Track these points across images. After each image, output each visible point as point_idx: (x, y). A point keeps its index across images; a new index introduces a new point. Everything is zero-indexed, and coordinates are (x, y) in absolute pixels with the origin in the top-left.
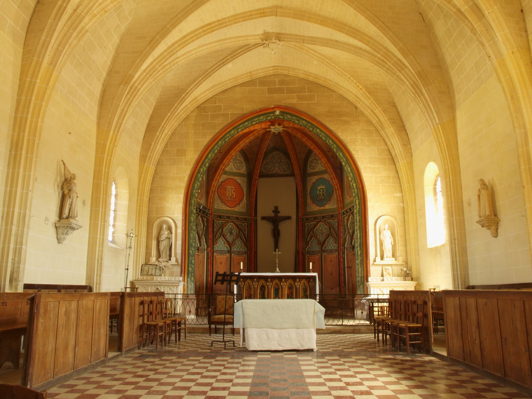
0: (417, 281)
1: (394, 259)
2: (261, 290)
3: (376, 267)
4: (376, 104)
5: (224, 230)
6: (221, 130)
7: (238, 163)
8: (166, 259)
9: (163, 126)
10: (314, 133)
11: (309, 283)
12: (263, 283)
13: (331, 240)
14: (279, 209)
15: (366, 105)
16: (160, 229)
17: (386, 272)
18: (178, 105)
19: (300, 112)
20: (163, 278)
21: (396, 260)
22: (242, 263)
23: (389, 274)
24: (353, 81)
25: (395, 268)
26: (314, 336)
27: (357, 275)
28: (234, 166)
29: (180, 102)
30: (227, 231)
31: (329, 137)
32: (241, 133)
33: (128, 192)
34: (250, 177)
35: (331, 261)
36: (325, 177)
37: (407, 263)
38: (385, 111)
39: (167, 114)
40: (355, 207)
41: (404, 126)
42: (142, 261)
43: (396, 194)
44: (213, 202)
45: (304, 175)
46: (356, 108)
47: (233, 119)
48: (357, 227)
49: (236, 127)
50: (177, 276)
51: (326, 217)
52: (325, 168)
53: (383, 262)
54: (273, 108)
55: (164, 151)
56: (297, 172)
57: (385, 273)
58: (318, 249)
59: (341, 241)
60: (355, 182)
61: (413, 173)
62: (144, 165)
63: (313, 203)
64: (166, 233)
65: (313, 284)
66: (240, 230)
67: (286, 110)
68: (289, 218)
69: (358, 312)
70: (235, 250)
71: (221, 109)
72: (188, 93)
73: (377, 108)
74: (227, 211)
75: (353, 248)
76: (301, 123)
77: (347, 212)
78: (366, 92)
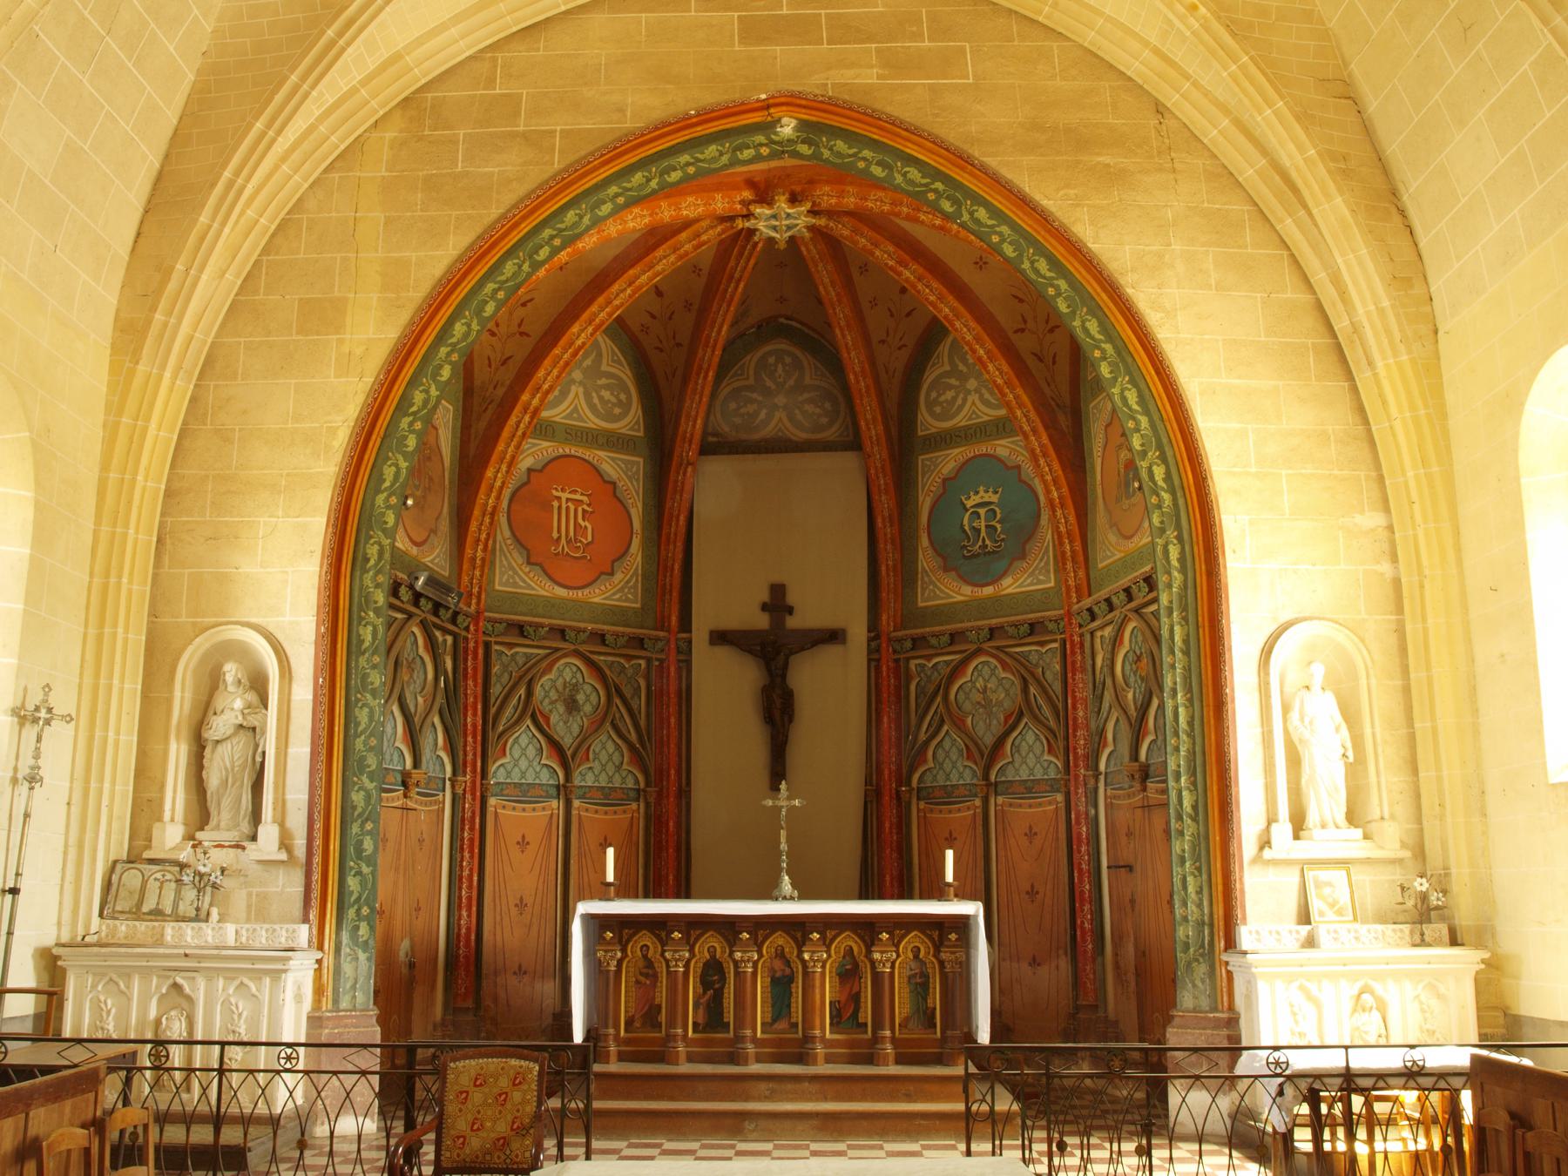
0: (1479, 945)
1: (1358, 833)
2: (705, 983)
3: (1272, 873)
5: (538, 691)
6: (515, 206)
7: (607, 387)
9: (231, 184)
11: (937, 950)
12: (712, 950)
14: (792, 598)
15: (1206, 94)
16: (212, 684)
18: (303, 79)
21: (1366, 837)
25: (1362, 876)
27: (1178, 911)
28: (584, 396)
30: (553, 695)
33: (30, 494)
36: (1002, 452)
37: (1420, 853)
38: (1304, 117)
39: (250, 126)
40: (1162, 579)
41: (1394, 193)
42: (111, 840)
43: (1358, 519)
44: (488, 563)
45: (905, 447)
46: (1160, 110)
47: (572, 158)
48: (1172, 678)
50: (283, 920)
51: (1003, 635)
52: (1003, 412)
53: (1302, 850)
55: (242, 308)
57: (1316, 905)
59: (1081, 742)
61: (1443, 415)
62: (131, 373)
64: (238, 704)
66: (613, 690)
67: (827, 118)
68: (834, 636)
69: (1190, 1103)
70: (590, 781)
71: (517, 114)
72: (351, 22)
73: (1270, 104)
74: (551, 604)
76: (899, 179)
77: (1111, 608)
78: (1216, 25)
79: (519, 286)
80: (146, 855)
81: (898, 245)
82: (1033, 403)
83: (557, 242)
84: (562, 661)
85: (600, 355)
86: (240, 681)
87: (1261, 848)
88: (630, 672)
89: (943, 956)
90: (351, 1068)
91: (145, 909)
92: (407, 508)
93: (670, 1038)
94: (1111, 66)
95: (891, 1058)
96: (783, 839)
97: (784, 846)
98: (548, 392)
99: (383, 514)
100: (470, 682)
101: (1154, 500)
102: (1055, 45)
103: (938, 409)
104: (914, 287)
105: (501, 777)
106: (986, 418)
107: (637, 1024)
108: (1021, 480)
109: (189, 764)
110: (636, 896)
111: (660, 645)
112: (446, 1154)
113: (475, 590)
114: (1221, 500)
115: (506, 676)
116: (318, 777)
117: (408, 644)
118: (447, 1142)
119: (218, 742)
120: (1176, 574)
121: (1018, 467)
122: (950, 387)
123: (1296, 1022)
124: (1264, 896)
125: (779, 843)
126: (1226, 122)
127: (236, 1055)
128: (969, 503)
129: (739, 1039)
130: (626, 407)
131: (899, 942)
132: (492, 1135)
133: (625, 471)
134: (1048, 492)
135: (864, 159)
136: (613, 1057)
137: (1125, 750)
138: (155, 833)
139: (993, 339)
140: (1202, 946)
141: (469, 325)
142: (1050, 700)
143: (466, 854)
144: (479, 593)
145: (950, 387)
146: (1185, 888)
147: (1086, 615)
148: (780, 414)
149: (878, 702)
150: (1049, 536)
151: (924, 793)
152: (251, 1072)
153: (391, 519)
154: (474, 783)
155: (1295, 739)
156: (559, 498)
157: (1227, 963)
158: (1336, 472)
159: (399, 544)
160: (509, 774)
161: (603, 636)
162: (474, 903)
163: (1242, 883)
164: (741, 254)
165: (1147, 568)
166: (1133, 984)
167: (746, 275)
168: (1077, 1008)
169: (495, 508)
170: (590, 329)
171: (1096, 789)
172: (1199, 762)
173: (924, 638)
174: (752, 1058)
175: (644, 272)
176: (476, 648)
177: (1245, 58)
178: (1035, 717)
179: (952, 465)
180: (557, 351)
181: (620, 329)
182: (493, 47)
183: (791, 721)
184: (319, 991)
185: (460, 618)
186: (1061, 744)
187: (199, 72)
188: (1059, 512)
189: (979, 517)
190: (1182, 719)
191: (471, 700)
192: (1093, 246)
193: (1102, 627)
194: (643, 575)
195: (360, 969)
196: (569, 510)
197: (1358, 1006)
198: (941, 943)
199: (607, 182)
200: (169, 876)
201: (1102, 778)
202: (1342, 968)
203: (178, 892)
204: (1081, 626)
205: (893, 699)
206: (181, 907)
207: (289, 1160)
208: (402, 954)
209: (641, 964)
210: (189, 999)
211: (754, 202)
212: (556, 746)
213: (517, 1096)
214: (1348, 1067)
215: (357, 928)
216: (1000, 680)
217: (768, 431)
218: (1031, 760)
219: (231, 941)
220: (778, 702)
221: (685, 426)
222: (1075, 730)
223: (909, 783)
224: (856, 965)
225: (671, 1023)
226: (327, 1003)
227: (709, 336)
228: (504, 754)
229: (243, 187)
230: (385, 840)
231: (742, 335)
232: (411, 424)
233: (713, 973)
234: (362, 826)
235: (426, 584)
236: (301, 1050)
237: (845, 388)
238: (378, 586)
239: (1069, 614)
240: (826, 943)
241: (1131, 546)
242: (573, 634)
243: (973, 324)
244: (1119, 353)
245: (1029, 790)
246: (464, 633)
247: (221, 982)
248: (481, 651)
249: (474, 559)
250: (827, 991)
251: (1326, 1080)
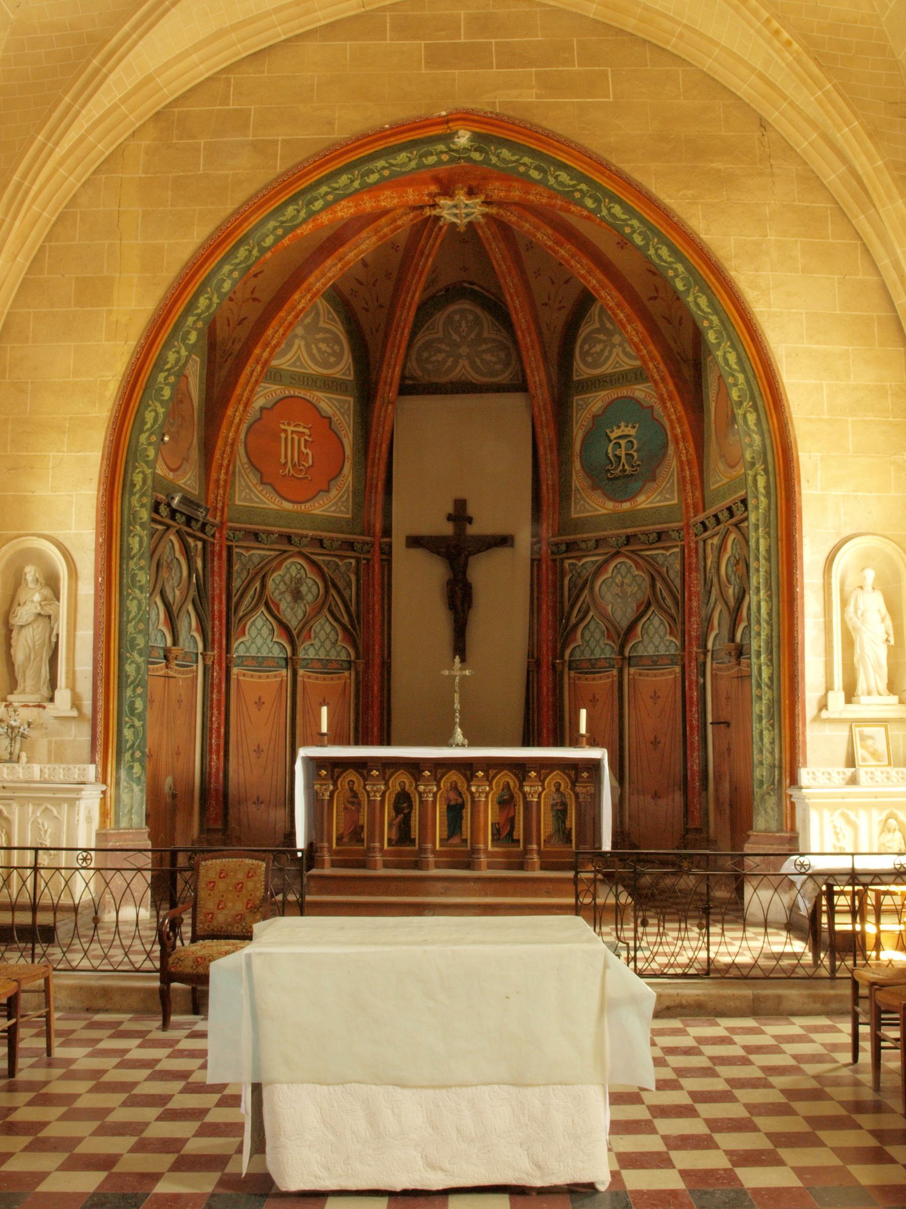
1: (894, 699)
2: (397, 809)
3: (828, 731)
4: (842, 103)
5: (270, 584)
6: (246, 203)
7: (324, 340)
8: (34, 698)
14: (471, 510)
15: (800, 112)
20: (20, 771)
22: (324, 710)
23: (874, 754)
24: (755, 13)
27: (756, 757)
28: (306, 350)
30: (282, 587)
31: (658, 234)
32: (325, 218)
34: (366, 390)
35: (655, 697)
38: (875, 135)
40: (751, 502)
44: (229, 484)
45: (565, 390)
46: (763, 124)
47: (290, 163)
48: (757, 579)
49: (303, 192)
50: (76, 761)
51: (633, 542)
52: (638, 363)
54: (446, 121)
56: (537, 377)
57: (860, 752)
58: (608, 654)
60: (755, 408)
63: (594, 488)
64: (37, 597)
65: (591, 789)
66: (329, 583)
67: (494, 130)
68: (505, 541)
69: (758, 898)
70: (311, 654)
74: (280, 515)
75: (740, 652)
76: (552, 181)
78: (805, 58)
79: (249, 268)
81: (555, 229)
82: (662, 357)
84: (289, 561)
86: (37, 580)
87: (820, 710)
88: (343, 569)
89: (578, 789)
92: (164, 443)
93: (370, 849)
94: (725, 88)
95: (537, 866)
96: (457, 700)
97: (457, 706)
98: (276, 346)
99: (146, 450)
103: (589, 359)
104: (568, 263)
105: (242, 651)
106: (627, 367)
107: (345, 840)
108: (653, 418)
110: (348, 744)
111: (366, 547)
112: (200, 926)
113: (220, 505)
115: (245, 572)
116: (99, 653)
118: (200, 917)
119: (22, 626)
120: (762, 498)
121: (652, 407)
122: (600, 341)
123: (838, 840)
124: (821, 744)
125: (453, 703)
126: (814, 136)
127: (44, 859)
128: (613, 436)
129: (422, 851)
131: (545, 779)
133: (338, 408)
134: (673, 428)
135: (525, 164)
136: (327, 864)
137: (725, 633)
140: (773, 783)
141: (210, 299)
142: (671, 593)
143: (215, 712)
144: (223, 508)
145: (600, 341)
146: (761, 739)
147: (701, 528)
148: (463, 362)
150: (674, 463)
151: (574, 665)
152: (58, 869)
153: (151, 453)
154: (220, 656)
155: (850, 628)
156: (285, 431)
157: (791, 796)
158: (891, 419)
159: (159, 471)
160: (248, 649)
161: (321, 541)
165: (743, 493)
167: (434, 251)
168: (687, 831)
169: (234, 440)
170: (309, 296)
171: (704, 663)
173: (575, 543)
176: (221, 551)
177: (829, 86)
178: (660, 607)
180: (282, 314)
182: (228, 70)
183: (470, 607)
184: (104, 814)
185: (208, 528)
186: (679, 627)
188: (681, 445)
189: (620, 447)
190: (764, 611)
192: (705, 237)
194: (354, 493)
196: (294, 442)
197: (885, 828)
201: (709, 654)
202: (873, 800)
204: (696, 535)
205: (550, 590)
207: (85, 936)
209: (348, 794)
211: (439, 194)
212: (285, 628)
213: (250, 885)
214: (853, 869)
215: (132, 767)
219: (37, 777)
220: (459, 593)
221: (386, 373)
222: (690, 617)
223: (562, 657)
224: (512, 796)
225: (371, 839)
226: (111, 823)
228: (244, 634)
231: (433, 297)
232: (166, 378)
233: (403, 801)
234: (134, 691)
236: (93, 853)
238: (142, 506)
239: (688, 526)
240: (489, 780)
242: (297, 540)
244: (722, 322)
245: (655, 663)
246: (211, 539)
248: (224, 554)
249: (218, 480)
250: (490, 815)
251: (837, 877)
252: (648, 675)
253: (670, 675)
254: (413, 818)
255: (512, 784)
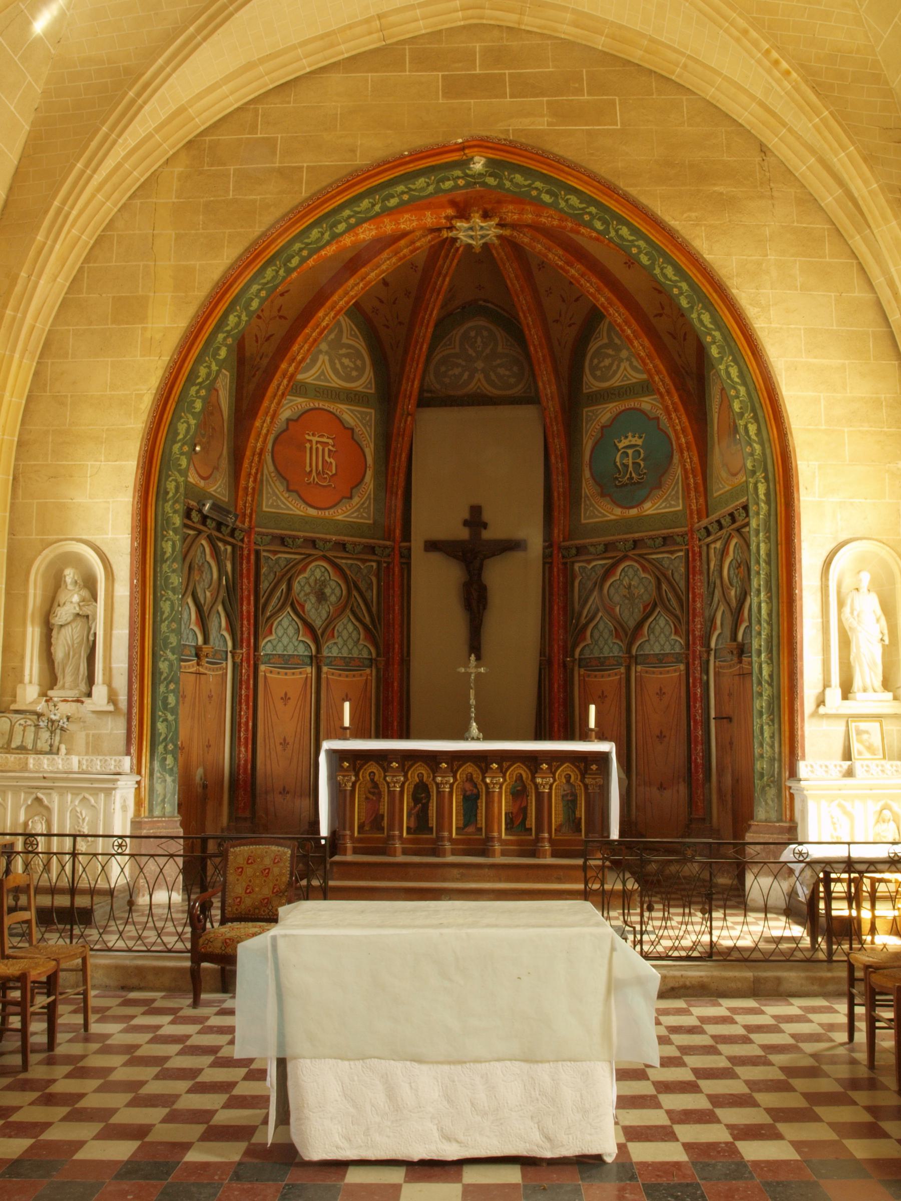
1: (890, 695)
2: (416, 799)
5: (296, 586)
6: (273, 226)
7: (346, 355)
8: (72, 694)
9: (59, 211)
10: (611, 240)
12: (420, 776)
13: (661, 622)
14: (487, 516)
15: (799, 138)
16: (55, 584)
17: (860, 741)
18: (112, 129)
19: (559, 162)
21: (895, 698)
23: (870, 748)
24: (755, 44)
26: (609, 1090)
27: (757, 751)
28: (328, 364)
29: (118, 121)
30: (307, 589)
32: (348, 240)
36: (646, 406)
38: (870, 159)
40: (753, 508)
44: (257, 492)
45: (574, 402)
46: (763, 149)
47: (316, 188)
48: (758, 582)
50: (112, 753)
51: (633, 546)
52: (645, 376)
53: (849, 707)
54: (462, 148)
55: (68, 305)
57: (856, 747)
59: (698, 626)
60: (756, 419)
63: (603, 495)
64: (76, 598)
65: (600, 781)
66: (351, 585)
67: (509, 156)
69: (758, 885)
70: (335, 652)
71: (274, 153)
73: (844, 148)
74: (305, 521)
75: (742, 651)
77: (721, 527)
78: (804, 87)
80: (13, 707)
81: (565, 250)
83: (305, 253)
84: (314, 564)
85: (341, 331)
86: (76, 582)
87: (818, 706)
90: (160, 852)
91: (13, 745)
93: (390, 838)
94: (727, 115)
95: (549, 853)
96: (472, 697)
97: (472, 701)
98: (301, 362)
99: (178, 459)
100: (245, 580)
101: (748, 449)
102: (684, 98)
103: (598, 373)
104: (578, 282)
105: (269, 650)
106: (634, 380)
107: (367, 828)
109: (41, 642)
111: (387, 551)
113: (248, 511)
114: (797, 450)
115: (272, 575)
117: (199, 553)
118: (229, 901)
119: (62, 626)
120: (763, 505)
121: (658, 418)
122: (609, 356)
123: (835, 829)
124: (818, 738)
126: (812, 160)
127: (82, 845)
128: (620, 446)
129: (440, 839)
130: (361, 371)
132: (259, 896)
133: (359, 419)
134: (678, 438)
135: (537, 189)
136: (349, 851)
137: (728, 633)
138: (19, 691)
139: (637, 321)
140: (773, 776)
141: (239, 317)
143: (244, 707)
144: (251, 514)
145: (609, 356)
146: (762, 733)
147: (703, 532)
148: (479, 376)
149: (551, 594)
150: (679, 471)
152: (95, 855)
153: (184, 462)
154: (248, 654)
156: (310, 441)
157: (790, 788)
158: (885, 429)
159: (191, 480)
160: (274, 648)
161: (344, 545)
162: (250, 742)
163: (803, 731)
164: (447, 256)
165: (744, 499)
166: (730, 803)
169: (262, 450)
170: (332, 314)
171: (708, 661)
172: (775, 643)
173: (585, 547)
174: (448, 852)
175: (373, 270)
176: (249, 555)
177: (826, 113)
179: (608, 415)
180: (307, 330)
181: (357, 311)
183: (484, 608)
184: (139, 803)
185: (237, 533)
186: (684, 628)
187: (33, 124)
188: (686, 454)
189: (628, 456)
191: (246, 593)
193: (715, 541)
195: (167, 788)
197: (880, 819)
198: (586, 772)
199: (342, 207)
200: (29, 722)
201: (712, 653)
202: (868, 792)
203: (36, 734)
204: (700, 540)
206: (39, 745)
207: (121, 918)
208: (198, 778)
209: (369, 785)
210: (48, 809)
214: (849, 857)
215: (165, 759)
216: (641, 579)
217: (472, 388)
218: (662, 639)
219: (75, 768)
222: (694, 617)
223: (573, 656)
225: (391, 827)
226: (144, 812)
227: (424, 318)
228: (271, 633)
229: (68, 214)
230: (184, 697)
232: (198, 392)
233: (421, 792)
234: (167, 686)
235: (211, 508)
236: (128, 840)
237: (528, 356)
238: (175, 512)
239: (692, 531)
240: (503, 771)
241: (736, 481)
242: (321, 544)
243: (622, 310)
246: (240, 544)
247: (69, 797)
248: (253, 557)
249: (246, 488)
250: (503, 805)
251: (835, 865)
252: (654, 673)
253: (674, 673)
254: (430, 808)
255: (524, 776)
